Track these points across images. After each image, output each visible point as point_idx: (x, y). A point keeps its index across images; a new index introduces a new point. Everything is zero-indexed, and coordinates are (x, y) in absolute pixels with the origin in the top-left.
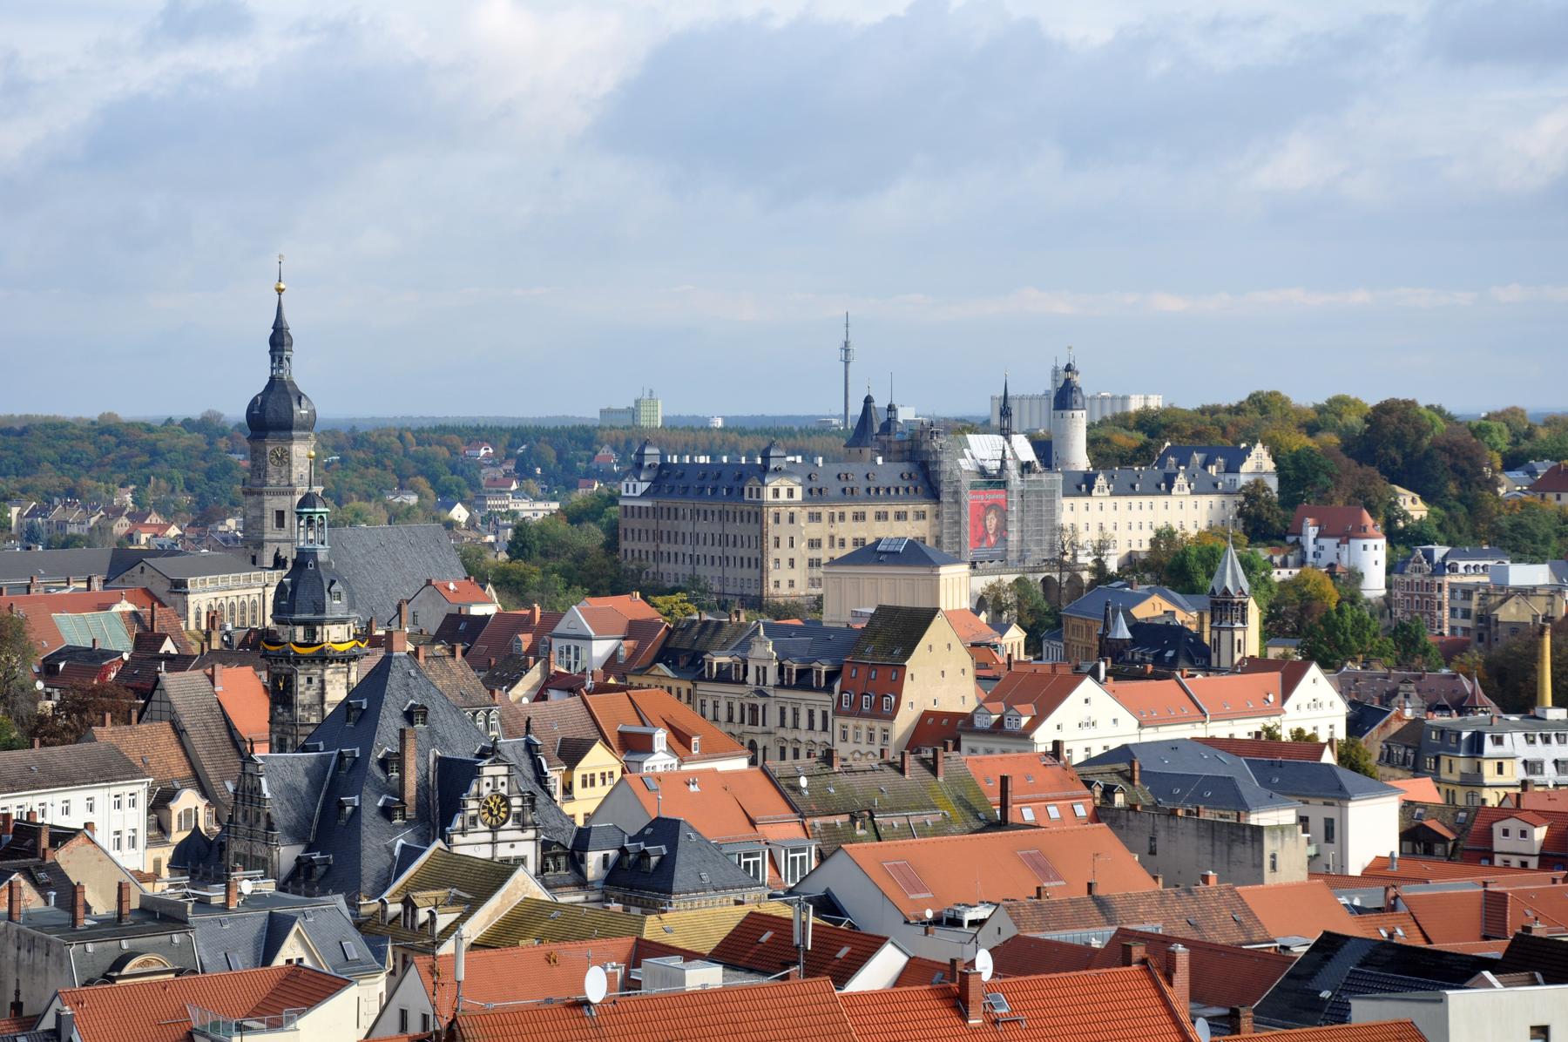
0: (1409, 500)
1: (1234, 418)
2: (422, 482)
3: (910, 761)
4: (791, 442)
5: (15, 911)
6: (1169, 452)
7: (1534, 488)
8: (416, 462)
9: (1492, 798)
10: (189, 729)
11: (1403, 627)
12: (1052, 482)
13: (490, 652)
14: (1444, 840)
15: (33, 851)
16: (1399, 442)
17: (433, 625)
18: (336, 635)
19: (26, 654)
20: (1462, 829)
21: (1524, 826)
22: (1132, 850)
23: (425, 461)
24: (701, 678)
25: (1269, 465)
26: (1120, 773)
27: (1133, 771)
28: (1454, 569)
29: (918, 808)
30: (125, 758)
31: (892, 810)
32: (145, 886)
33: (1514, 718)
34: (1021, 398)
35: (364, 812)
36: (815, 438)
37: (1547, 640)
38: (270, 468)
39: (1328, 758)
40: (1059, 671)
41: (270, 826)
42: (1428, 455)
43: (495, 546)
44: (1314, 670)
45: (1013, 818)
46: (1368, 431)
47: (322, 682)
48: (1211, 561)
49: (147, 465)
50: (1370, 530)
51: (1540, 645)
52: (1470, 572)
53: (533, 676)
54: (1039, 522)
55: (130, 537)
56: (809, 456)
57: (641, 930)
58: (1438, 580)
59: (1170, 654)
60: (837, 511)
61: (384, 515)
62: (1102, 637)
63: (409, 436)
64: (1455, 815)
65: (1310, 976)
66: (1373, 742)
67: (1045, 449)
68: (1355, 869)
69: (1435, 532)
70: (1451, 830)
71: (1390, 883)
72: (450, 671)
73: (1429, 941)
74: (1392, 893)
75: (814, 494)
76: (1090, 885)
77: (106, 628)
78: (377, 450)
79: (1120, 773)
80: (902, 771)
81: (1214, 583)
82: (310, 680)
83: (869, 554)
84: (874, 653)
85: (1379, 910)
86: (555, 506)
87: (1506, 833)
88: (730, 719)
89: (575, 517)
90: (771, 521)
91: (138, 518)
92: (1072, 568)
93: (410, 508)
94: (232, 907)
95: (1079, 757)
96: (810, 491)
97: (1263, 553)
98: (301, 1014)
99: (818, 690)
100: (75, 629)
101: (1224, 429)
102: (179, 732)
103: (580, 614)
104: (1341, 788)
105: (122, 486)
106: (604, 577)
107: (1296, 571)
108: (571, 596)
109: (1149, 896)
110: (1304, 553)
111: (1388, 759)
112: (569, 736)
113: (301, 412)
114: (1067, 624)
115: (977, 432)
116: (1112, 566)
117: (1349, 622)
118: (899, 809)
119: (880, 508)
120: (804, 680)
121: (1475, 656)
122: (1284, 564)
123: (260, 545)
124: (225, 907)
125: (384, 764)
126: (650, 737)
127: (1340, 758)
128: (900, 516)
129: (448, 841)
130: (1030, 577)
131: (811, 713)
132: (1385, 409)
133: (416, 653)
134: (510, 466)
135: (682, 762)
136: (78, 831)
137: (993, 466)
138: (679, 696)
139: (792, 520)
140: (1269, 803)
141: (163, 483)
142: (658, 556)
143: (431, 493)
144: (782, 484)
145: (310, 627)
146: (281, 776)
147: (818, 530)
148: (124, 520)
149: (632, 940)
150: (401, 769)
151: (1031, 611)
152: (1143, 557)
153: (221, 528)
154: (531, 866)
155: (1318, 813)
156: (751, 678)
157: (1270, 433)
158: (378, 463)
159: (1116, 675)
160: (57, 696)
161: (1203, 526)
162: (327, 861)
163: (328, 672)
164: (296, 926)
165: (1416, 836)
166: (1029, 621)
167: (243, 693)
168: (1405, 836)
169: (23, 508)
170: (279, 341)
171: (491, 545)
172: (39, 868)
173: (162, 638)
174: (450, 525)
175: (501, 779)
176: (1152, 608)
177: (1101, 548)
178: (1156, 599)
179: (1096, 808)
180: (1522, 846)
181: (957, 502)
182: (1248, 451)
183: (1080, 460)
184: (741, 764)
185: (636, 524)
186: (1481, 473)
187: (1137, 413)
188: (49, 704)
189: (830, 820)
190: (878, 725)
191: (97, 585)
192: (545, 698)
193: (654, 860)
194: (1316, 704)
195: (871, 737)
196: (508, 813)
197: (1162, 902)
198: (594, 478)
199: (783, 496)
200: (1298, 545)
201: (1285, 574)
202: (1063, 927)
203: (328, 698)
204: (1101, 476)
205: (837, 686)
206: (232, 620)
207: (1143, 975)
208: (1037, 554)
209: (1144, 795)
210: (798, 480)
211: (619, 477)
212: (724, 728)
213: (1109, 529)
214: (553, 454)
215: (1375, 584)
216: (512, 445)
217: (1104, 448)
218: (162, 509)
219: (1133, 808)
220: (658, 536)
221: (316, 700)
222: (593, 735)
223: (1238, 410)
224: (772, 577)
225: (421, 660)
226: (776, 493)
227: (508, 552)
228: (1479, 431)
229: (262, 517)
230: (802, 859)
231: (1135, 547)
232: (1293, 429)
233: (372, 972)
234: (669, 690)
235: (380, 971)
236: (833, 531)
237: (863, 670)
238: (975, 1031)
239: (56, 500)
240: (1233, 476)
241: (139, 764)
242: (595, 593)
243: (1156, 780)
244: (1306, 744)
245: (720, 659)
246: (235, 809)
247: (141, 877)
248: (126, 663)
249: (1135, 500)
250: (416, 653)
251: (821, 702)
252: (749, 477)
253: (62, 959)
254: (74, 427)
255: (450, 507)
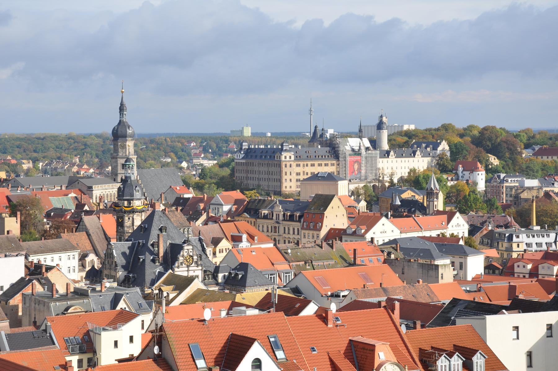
0: (493, 159)
1: (437, 132)
2: (172, 154)
3: (324, 244)
4: (292, 141)
5: (34, 292)
6: (414, 143)
7: (534, 155)
8: (163, 148)
9: (515, 255)
10: (92, 234)
11: (490, 200)
12: (376, 154)
13: (190, 209)
14: (498, 269)
15: (41, 273)
16: (490, 139)
17: (172, 200)
18: (137, 204)
19: (40, 210)
20: (504, 264)
21: (524, 264)
22: (396, 272)
23: (173, 147)
24: (258, 218)
25: (447, 148)
26: (393, 248)
27: (397, 247)
28: (507, 181)
29: (327, 259)
30: (71, 244)
31: (318, 260)
32: (76, 284)
33: (523, 229)
34: (365, 126)
35: (146, 261)
36: (301, 139)
37: (534, 204)
38: (120, 150)
39: (461, 242)
40: (376, 215)
41: (116, 266)
42: (499, 144)
43: (194, 175)
44: (458, 214)
45: (358, 262)
46: (480, 136)
47: (133, 219)
48: (427, 178)
49: (83, 149)
50: (480, 168)
51: (532, 206)
52: (512, 182)
53: (204, 217)
54: (372, 167)
55: (78, 173)
56: (296, 146)
57: (235, 299)
58: (502, 185)
59: (413, 209)
60: (305, 163)
61: (160, 165)
62: (391, 204)
63: (168, 139)
64: (502, 261)
65: (448, 312)
66: (477, 238)
67: (374, 143)
68: (469, 278)
69: (502, 169)
70: (501, 266)
71: (478, 283)
72: (176, 216)
73: (491, 301)
74: (479, 286)
75: (298, 158)
76: (381, 284)
77: (67, 202)
78: (158, 144)
79: (393, 248)
80: (321, 247)
81: (427, 186)
82: (129, 219)
83: (315, 177)
84: (314, 209)
85: (475, 291)
86: (215, 162)
87: (518, 266)
88: (268, 231)
89: (221, 166)
90: (284, 166)
91: (80, 166)
92: (382, 182)
93: (168, 163)
94: (103, 291)
95: (381, 243)
96: (297, 157)
97: (445, 176)
98: (123, 325)
99: (296, 221)
100: (57, 202)
101: (433, 136)
102: (89, 235)
103: (220, 196)
104: (465, 252)
105: (75, 156)
106: (227, 184)
107: (455, 182)
108: (218, 191)
109: (400, 287)
110: (458, 176)
111: (482, 243)
112: (215, 236)
113: (129, 131)
114: (382, 200)
115: (351, 137)
116: (395, 181)
117: (472, 199)
118: (320, 260)
119: (319, 162)
120: (291, 218)
121: (513, 210)
122: (452, 180)
123: (116, 175)
124: (101, 291)
125: (153, 245)
126: (241, 237)
127: (466, 243)
128: (326, 165)
129: (173, 270)
130: (369, 185)
131: (294, 229)
132: (485, 129)
133: (165, 210)
134: (201, 149)
135: (251, 245)
136: (54, 267)
137: (356, 148)
138: (251, 223)
139: (291, 166)
140: (442, 257)
141: (88, 155)
142: (247, 178)
143: (175, 158)
144: (288, 154)
145: (129, 201)
146: (120, 249)
147: (298, 170)
148: (76, 167)
149: (230, 302)
150: (158, 247)
151: (369, 196)
152: (406, 178)
153: (107, 170)
154: (200, 279)
155: (457, 260)
156: (274, 217)
157: (448, 137)
158: (158, 148)
159: (394, 216)
160: (51, 224)
161: (425, 168)
162: (134, 275)
163: (135, 216)
164: (123, 297)
165: (489, 268)
166: (368, 199)
167: (109, 222)
168: (486, 268)
169: (44, 163)
170: (122, 109)
171: (194, 175)
172: (42, 278)
173: (84, 205)
174: (181, 168)
175: (190, 250)
176: (408, 195)
177: (392, 175)
178: (409, 191)
179: (385, 259)
180: (524, 271)
181: (345, 160)
182: (440, 143)
183: (385, 146)
184: (271, 245)
185: (240, 168)
186: (517, 150)
187: (405, 131)
188: (48, 226)
189: (298, 263)
190: (315, 233)
191: (64, 188)
192: (207, 224)
193: (240, 276)
194: (458, 225)
195: (313, 237)
196: (193, 261)
197: (404, 289)
198: (228, 153)
199: (288, 159)
200: (456, 174)
201: (452, 183)
202: (372, 297)
203: (135, 224)
204: (392, 151)
205: (302, 220)
206: (107, 199)
207: (385, 311)
208: (371, 177)
209: (401, 255)
210: (293, 153)
211: (236, 152)
212: (266, 234)
213: (394, 169)
214: (215, 145)
215: (481, 186)
216: (201, 142)
217: (393, 142)
218: (88, 163)
219: (397, 259)
220: (247, 172)
221: (131, 225)
222: (223, 236)
223: (438, 130)
224: (284, 184)
225: (167, 212)
226: (286, 157)
227: (199, 177)
228: (517, 136)
229: (117, 166)
230: (289, 276)
231: (403, 175)
232: (455, 136)
233: (146, 312)
234: (248, 222)
235: (151, 311)
236: (304, 170)
237: (311, 215)
238: (330, 328)
239: (54, 160)
240: (435, 151)
241: (76, 245)
242: (226, 190)
243: (405, 251)
244: (455, 238)
245: (265, 212)
246: (105, 260)
247: (75, 282)
248: (73, 213)
249: (403, 159)
250: (165, 210)
251: (297, 225)
252: (277, 152)
253: (49, 308)
254: (60, 137)
255: (181, 162)
